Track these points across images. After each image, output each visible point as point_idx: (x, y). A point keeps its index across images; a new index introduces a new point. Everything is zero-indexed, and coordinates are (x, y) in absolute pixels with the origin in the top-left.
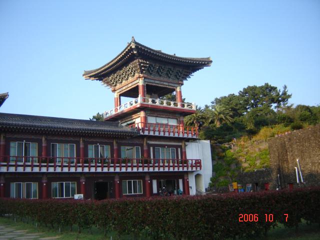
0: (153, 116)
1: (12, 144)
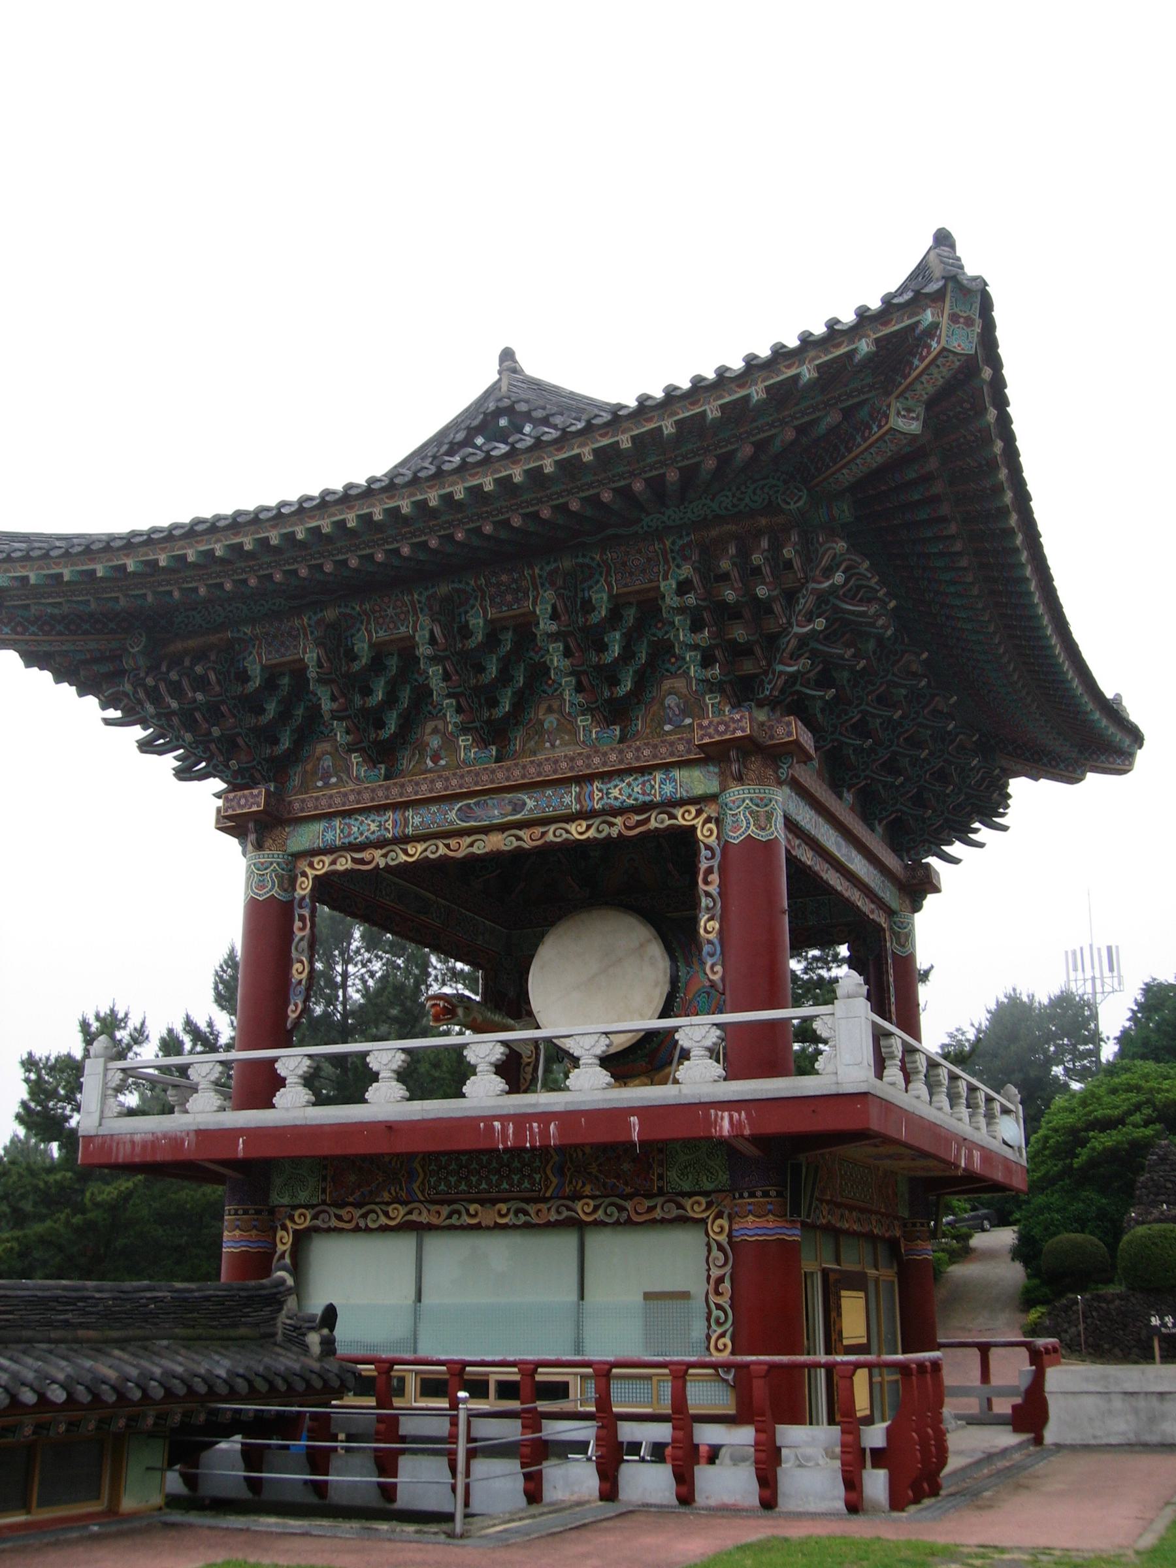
0: (550, 1226)
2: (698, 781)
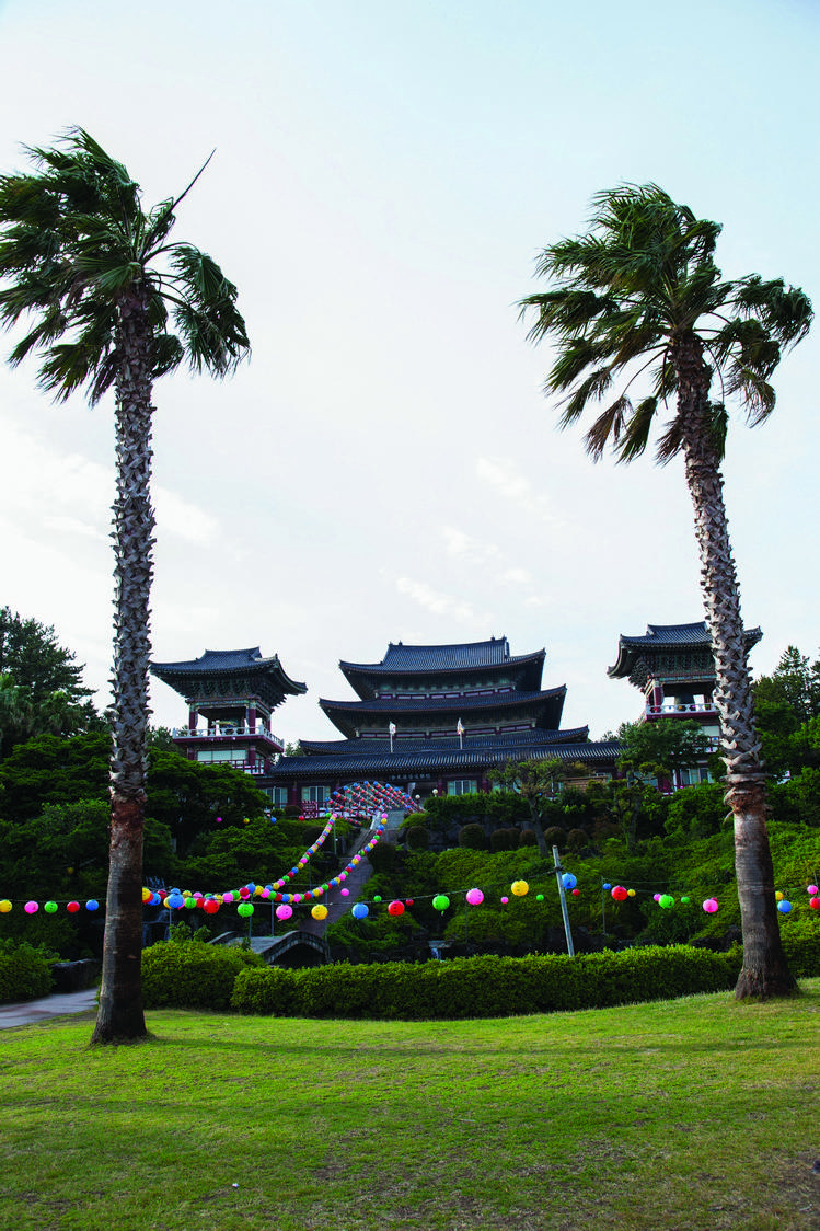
1: (450, 784)
2: (246, 701)
